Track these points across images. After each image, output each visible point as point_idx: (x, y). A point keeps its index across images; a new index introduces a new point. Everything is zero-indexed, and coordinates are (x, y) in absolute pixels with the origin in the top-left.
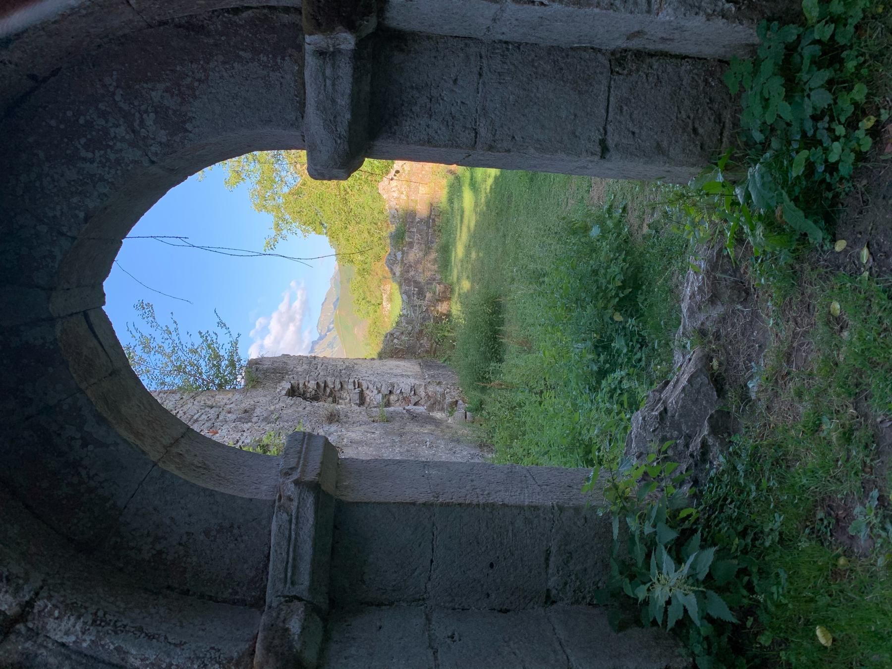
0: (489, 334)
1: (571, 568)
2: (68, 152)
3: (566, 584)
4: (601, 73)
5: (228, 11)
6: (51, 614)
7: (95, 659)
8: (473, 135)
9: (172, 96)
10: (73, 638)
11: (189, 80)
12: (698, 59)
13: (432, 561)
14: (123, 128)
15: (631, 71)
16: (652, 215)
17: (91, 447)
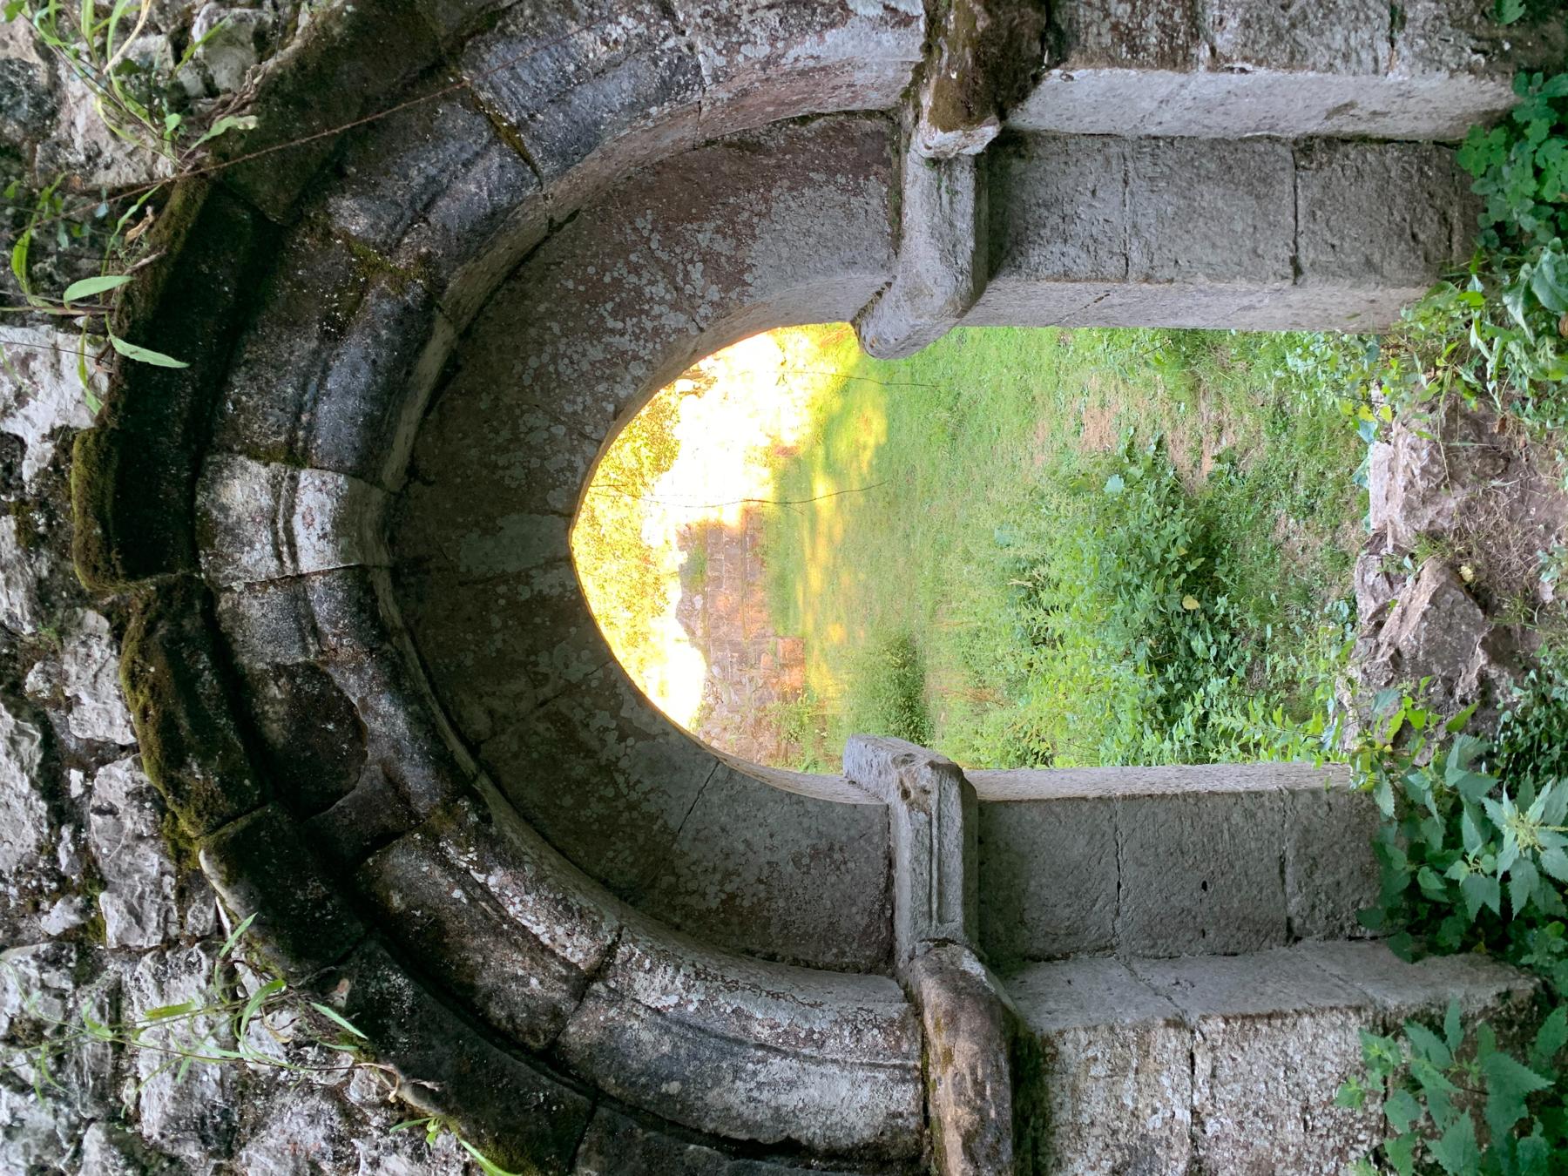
0: (901, 701)
1: (1318, 882)
2: (591, 322)
3: (1313, 907)
4: (1283, 169)
5: (793, 121)
6: (640, 966)
7: (703, 1031)
8: (1123, 262)
9: (725, 238)
10: (674, 1000)
11: (746, 215)
12: (1410, 143)
13: (1119, 886)
14: (661, 285)
15: (1321, 164)
16: (1218, 441)
17: (631, 741)
